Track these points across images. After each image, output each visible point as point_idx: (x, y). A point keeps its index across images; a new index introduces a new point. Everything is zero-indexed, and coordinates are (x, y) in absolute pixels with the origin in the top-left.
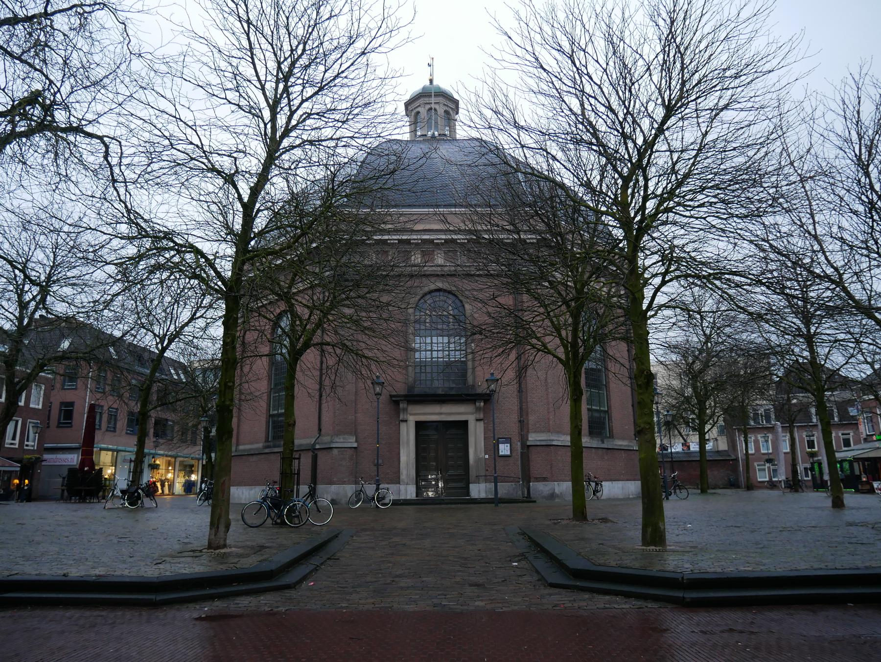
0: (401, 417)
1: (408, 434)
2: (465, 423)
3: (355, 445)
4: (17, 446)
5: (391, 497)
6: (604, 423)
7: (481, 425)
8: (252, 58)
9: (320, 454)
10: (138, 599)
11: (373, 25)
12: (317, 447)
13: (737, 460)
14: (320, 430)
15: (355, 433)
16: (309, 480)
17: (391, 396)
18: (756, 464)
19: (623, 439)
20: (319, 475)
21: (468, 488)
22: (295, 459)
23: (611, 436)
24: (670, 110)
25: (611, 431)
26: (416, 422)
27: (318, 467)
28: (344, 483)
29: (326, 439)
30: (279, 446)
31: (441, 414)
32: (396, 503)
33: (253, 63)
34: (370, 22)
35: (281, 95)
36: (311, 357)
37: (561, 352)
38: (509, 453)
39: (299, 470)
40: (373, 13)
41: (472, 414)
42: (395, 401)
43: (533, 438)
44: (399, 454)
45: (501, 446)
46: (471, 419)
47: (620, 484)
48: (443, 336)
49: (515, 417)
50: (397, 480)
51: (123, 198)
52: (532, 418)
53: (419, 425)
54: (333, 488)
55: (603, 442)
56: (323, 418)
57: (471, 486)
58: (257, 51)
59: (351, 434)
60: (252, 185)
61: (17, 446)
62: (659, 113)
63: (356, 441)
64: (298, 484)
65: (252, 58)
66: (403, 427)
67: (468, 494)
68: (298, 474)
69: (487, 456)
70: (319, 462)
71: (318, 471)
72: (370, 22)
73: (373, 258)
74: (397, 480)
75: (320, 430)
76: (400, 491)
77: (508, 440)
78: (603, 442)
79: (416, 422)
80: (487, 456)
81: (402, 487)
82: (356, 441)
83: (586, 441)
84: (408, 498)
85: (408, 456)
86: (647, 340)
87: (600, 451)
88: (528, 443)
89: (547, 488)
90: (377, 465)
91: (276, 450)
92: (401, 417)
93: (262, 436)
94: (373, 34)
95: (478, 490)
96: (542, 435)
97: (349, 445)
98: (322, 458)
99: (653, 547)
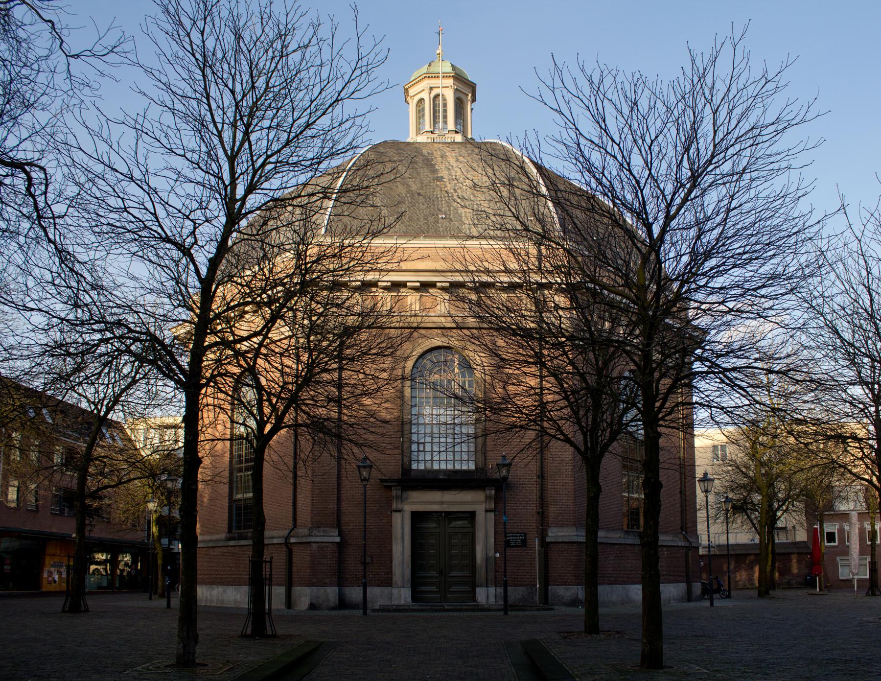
0: (394, 506)
3: (338, 539)
5: (380, 603)
7: (491, 515)
9: (295, 550)
10: (539, 566)
12: (293, 540)
17: (382, 481)
20: (295, 576)
22: (266, 562)
27: (294, 565)
28: (325, 585)
30: (246, 538)
32: (384, 609)
33: (209, 105)
37: (579, 439)
39: (271, 575)
41: (481, 503)
42: (387, 484)
46: (480, 510)
49: (533, 508)
50: (387, 582)
51: (51, 236)
52: (553, 510)
53: (418, 518)
56: (299, 505)
57: (477, 589)
60: (211, 256)
63: (339, 535)
64: (270, 585)
66: (397, 518)
67: (474, 598)
68: (271, 562)
69: (498, 555)
70: (295, 559)
71: (294, 570)
73: (358, 302)
74: (387, 582)
76: (391, 594)
80: (498, 555)
81: (395, 591)
82: (339, 535)
84: (402, 603)
88: (548, 540)
89: (569, 593)
90: (364, 564)
91: (243, 542)
92: (394, 506)
93: (225, 525)
95: (485, 595)
97: (331, 540)
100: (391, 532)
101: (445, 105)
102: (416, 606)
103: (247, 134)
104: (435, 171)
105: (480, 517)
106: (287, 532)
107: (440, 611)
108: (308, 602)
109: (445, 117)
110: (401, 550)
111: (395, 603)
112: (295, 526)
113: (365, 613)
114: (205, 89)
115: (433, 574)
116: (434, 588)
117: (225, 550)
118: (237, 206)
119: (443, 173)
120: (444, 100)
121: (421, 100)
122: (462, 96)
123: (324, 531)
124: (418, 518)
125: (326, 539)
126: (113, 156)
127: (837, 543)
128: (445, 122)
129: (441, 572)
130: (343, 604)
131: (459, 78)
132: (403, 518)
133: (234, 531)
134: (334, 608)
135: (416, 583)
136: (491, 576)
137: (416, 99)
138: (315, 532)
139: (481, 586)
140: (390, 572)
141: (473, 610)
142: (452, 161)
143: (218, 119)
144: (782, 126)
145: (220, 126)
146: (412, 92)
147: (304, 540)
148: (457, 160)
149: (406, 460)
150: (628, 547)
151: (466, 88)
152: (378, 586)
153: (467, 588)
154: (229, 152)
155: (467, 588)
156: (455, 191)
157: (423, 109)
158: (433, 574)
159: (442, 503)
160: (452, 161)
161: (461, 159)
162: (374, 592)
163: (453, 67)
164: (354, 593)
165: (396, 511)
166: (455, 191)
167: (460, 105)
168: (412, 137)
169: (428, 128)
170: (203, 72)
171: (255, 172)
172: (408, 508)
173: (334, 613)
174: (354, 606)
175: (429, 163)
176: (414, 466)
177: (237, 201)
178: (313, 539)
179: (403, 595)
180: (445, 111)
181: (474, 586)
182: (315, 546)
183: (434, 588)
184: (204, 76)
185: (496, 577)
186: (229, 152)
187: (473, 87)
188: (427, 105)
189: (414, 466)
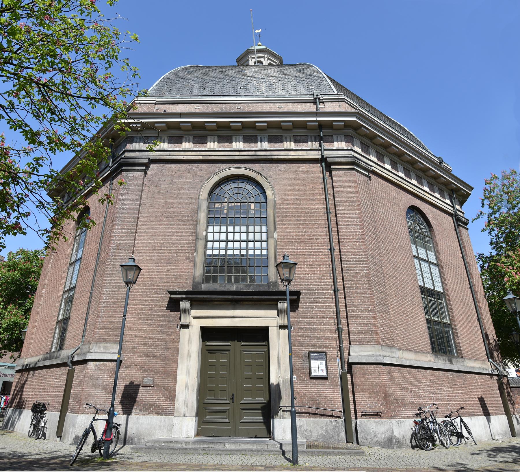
1: (190, 343)
6: (448, 339)
16: (59, 405)
19: (474, 359)
23: (460, 356)
25: (458, 349)
26: (4, 382)
38: (324, 374)
43: (358, 353)
45: (314, 363)
46: (273, 325)
48: (240, 225)
50: (168, 409)
53: (208, 334)
55: (451, 363)
74: (168, 409)
76: (172, 425)
77: (322, 355)
78: (451, 363)
79: (4, 382)
81: (175, 420)
85: (188, 374)
86: (123, 411)
92: (183, 321)
96: (369, 348)
123: (105, 348)
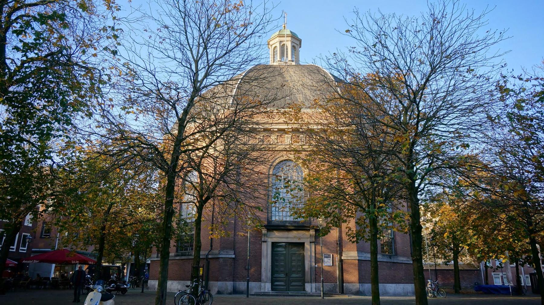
0: (263, 239)
2: (302, 245)
3: (233, 256)
4: (14, 250)
8: (186, 33)
9: (212, 262)
11: (258, 17)
12: (210, 257)
13: (480, 270)
14: (212, 246)
15: (234, 249)
18: (493, 273)
19: (404, 256)
21: (304, 286)
23: (396, 254)
24: (433, 70)
25: (396, 251)
28: (226, 280)
29: (216, 252)
31: (287, 238)
33: (186, 36)
34: (256, 17)
35: (202, 55)
36: (211, 201)
40: (258, 11)
44: (261, 262)
47: (401, 286)
50: (259, 279)
53: (274, 245)
54: (219, 283)
58: (189, 30)
59: (231, 249)
61: (14, 250)
62: (427, 69)
65: (186, 33)
66: (264, 245)
67: (304, 290)
71: (210, 272)
72: (256, 17)
74: (259, 279)
75: (212, 246)
81: (263, 284)
83: (380, 257)
84: (266, 291)
87: (389, 264)
94: (258, 22)
97: (230, 256)
98: (212, 264)
99: (539, 255)
100: (261, 252)
101: (287, 49)
102: (274, 293)
103: (206, 48)
104: (284, 78)
105: (307, 246)
106: (207, 252)
107: (287, 296)
108: (216, 290)
109: (287, 54)
110: (266, 262)
111: (262, 291)
112: (211, 249)
113: (248, 296)
114: (185, 28)
115: (282, 275)
116: (282, 283)
117: (174, 261)
118: (198, 84)
119: (288, 78)
120: (287, 47)
121: (275, 47)
122: (295, 45)
124: (274, 245)
125: (227, 256)
126: (137, 58)
127: (23, 234)
128: (287, 57)
129: (287, 275)
130: (235, 291)
131: (294, 36)
132: (267, 245)
133: (179, 251)
134: (230, 294)
135: (273, 281)
136: (313, 277)
137: (274, 46)
138: (222, 252)
139: (308, 282)
140: (260, 274)
141: (305, 296)
142: (292, 73)
143: (191, 43)
144: (485, 42)
145: (191, 46)
146: (271, 43)
147: (216, 256)
148: (294, 73)
149: (270, 215)
150: (384, 264)
151: (297, 42)
152: (254, 281)
153: (300, 283)
154: (195, 58)
155: (300, 283)
156: (294, 86)
157: (277, 51)
158: (282, 275)
159: (287, 238)
160: (292, 73)
161: (296, 72)
162: (252, 284)
163: (291, 32)
164: (242, 285)
165: (264, 242)
166: (294, 86)
167: (294, 47)
168: (271, 63)
169: (279, 59)
170: (184, 20)
171: (209, 67)
172: (270, 241)
173: (231, 296)
174: (241, 293)
175: (281, 74)
176: (273, 219)
177: (198, 81)
178: (221, 256)
179: (267, 287)
180: (287, 52)
181: (304, 282)
182: (221, 260)
183: (282, 283)
184: (184, 22)
185: (315, 278)
186: (195, 58)
187: (300, 41)
188: (278, 49)
189: (273, 219)
